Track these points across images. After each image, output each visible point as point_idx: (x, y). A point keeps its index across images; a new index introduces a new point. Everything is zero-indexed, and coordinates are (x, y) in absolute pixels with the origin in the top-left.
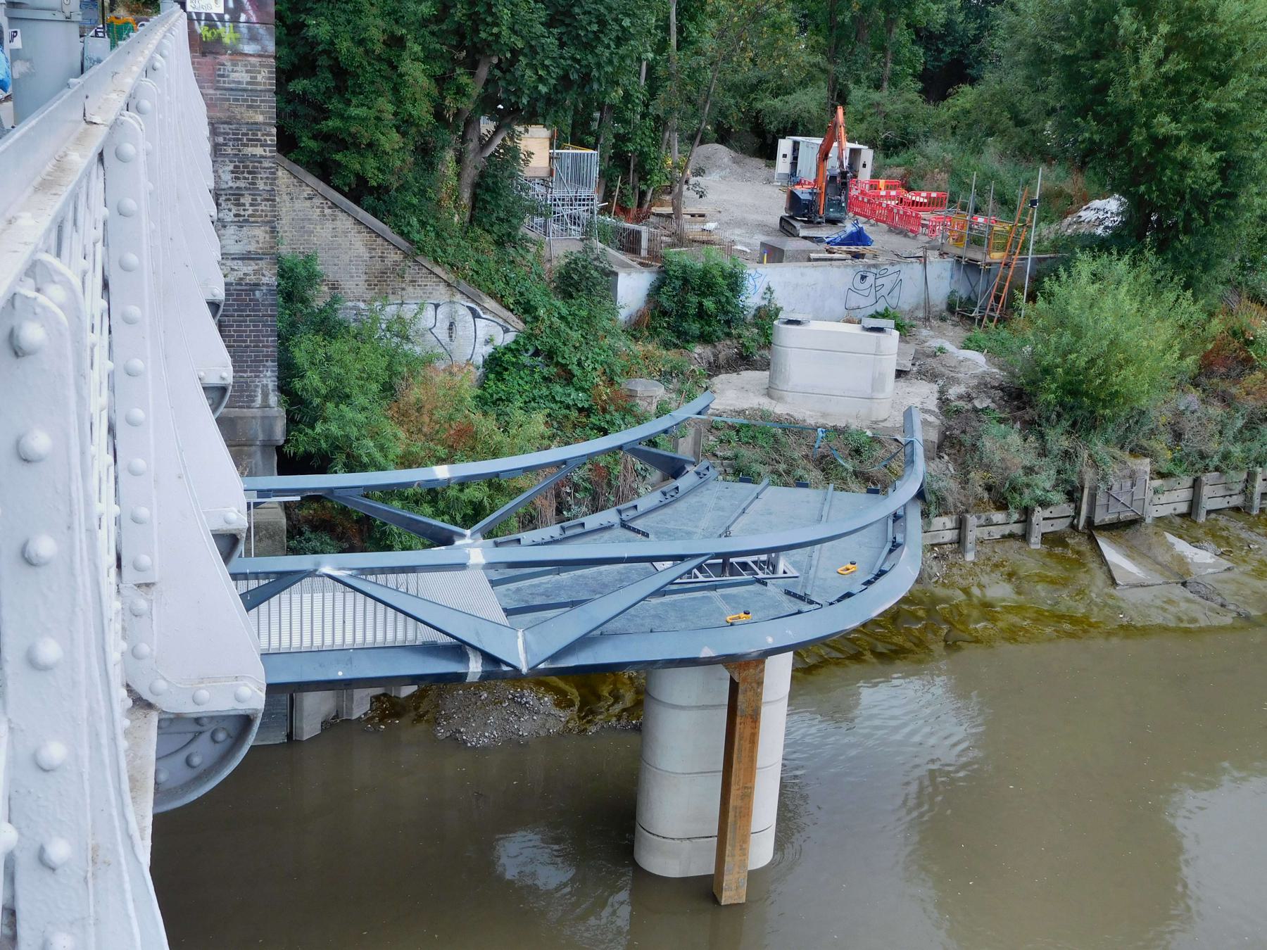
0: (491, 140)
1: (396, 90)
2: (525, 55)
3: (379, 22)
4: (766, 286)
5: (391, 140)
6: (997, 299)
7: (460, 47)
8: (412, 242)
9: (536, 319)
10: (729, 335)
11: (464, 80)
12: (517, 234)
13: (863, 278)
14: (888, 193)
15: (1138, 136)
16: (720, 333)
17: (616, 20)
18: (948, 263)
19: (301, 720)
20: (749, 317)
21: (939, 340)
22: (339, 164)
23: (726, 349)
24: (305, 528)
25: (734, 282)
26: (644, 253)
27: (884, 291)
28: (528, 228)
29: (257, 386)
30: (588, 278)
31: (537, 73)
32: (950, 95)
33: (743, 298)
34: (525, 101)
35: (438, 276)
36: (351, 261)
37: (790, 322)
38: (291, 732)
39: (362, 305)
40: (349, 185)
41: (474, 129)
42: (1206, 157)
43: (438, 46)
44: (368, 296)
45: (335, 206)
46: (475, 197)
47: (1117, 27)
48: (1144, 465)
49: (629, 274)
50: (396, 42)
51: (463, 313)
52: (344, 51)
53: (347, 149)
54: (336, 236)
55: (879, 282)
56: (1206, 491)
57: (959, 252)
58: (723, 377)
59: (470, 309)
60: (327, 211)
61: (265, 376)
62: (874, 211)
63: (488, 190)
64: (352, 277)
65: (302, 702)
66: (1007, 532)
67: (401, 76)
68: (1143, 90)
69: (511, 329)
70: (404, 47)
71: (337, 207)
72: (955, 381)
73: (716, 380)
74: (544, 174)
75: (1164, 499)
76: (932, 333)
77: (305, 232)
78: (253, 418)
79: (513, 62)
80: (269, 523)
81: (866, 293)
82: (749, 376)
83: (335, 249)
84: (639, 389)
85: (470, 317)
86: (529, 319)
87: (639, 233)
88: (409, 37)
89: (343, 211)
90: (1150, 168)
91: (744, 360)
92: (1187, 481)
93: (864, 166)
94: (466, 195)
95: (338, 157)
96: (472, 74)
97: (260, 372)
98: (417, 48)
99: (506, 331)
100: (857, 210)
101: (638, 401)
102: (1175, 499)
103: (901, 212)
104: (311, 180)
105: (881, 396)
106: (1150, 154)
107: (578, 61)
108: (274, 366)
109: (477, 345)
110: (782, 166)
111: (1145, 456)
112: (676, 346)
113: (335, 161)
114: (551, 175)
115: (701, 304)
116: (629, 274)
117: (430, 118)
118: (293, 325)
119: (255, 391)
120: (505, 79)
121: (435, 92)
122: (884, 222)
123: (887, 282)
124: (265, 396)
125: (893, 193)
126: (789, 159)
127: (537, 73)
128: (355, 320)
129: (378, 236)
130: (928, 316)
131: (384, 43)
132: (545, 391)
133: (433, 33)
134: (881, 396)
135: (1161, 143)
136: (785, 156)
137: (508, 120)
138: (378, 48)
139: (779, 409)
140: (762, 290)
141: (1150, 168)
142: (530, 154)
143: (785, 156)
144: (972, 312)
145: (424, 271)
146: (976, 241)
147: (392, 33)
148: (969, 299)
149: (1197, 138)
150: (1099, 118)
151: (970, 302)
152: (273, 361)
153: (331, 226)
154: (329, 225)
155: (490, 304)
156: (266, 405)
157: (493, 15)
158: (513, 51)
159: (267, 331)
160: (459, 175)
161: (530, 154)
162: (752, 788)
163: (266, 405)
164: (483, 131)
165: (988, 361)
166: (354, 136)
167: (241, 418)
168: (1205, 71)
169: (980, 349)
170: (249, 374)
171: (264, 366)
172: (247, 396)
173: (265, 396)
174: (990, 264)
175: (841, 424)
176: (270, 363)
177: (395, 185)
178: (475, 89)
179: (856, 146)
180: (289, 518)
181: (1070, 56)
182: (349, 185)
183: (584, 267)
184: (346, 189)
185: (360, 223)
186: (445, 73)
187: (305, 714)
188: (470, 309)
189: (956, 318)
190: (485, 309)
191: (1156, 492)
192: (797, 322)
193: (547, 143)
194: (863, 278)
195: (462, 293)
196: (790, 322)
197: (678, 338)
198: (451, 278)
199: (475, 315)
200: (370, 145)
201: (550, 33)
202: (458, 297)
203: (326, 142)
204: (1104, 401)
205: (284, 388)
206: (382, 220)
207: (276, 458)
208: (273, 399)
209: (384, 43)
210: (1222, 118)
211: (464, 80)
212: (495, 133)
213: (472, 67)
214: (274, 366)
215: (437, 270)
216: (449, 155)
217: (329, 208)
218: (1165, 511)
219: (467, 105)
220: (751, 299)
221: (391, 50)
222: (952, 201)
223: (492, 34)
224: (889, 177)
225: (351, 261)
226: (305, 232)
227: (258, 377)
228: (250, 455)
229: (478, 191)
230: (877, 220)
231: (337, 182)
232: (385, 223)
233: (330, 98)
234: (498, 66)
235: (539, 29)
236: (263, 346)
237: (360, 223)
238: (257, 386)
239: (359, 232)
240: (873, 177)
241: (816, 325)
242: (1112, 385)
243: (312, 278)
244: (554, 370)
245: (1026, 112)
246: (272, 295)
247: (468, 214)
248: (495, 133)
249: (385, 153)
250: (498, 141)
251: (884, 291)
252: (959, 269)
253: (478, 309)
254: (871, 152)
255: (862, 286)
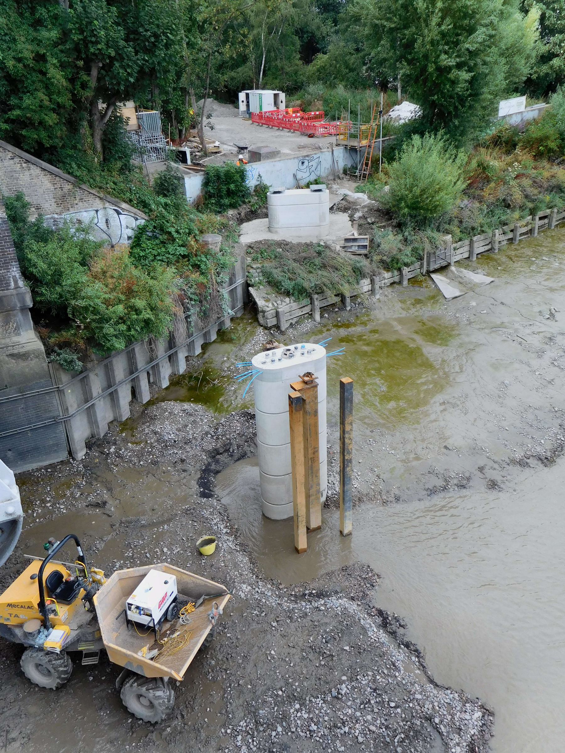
0: (106, 112)
1: (47, 87)
2: (117, 60)
3: (29, 47)
4: (258, 174)
5: (51, 119)
6: (367, 165)
7: (79, 58)
8: (76, 177)
9: (151, 210)
10: (244, 202)
11: (85, 78)
12: (129, 165)
13: (303, 163)
14: (296, 115)
15: (431, 68)
16: (240, 203)
17: (164, 33)
18: (341, 149)
19: (74, 444)
20: (252, 191)
21: (343, 190)
22: (24, 137)
23: (244, 210)
24: (56, 348)
25: (242, 174)
26: (189, 162)
27: (313, 169)
28: (135, 161)
29: (10, 277)
30: (172, 184)
31: (126, 71)
32: (314, 59)
33: (247, 182)
34: (122, 88)
35: (94, 195)
36: (44, 192)
37: (275, 193)
38: (70, 451)
39: (56, 216)
40: (34, 148)
41: (95, 107)
42: (465, 75)
43: (66, 59)
44: (58, 210)
45: (27, 161)
46: (104, 147)
47: (416, 9)
48: (449, 237)
49: (190, 178)
50: (40, 58)
51: (111, 213)
52: (11, 68)
53: (27, 127)
54: (32, 179)
55: (310, 164)
56: (476, 245)
57: (345, 143)
58: (245, 225)
59: (115, 210)
60: (24, 165)
61: (13, 271)
62: (291, 125)
63: (110, 142)
64: (47, 201)
65: (73, 436)
66: (392, 281)
67: (49, 79)
68: (432, 42)
69: (139, 218)
70: (45, 61)
71: (29, 162)
72: (357, 210)
73: (242, 226)
74: (136, 127)
75: (458, 252)
76: (338, 186)
77: (14, 179)
78: (11, 295)
79: (111, 65)
80: (34, 350)
81: (305, 171)
82: (256, 223)
83: (33, 186)
84: (210, 240)
85: (116, 215)
86: (147, 211)
87: (185, 152)
88: (48, 54)
89: (33, 164)
90: (436, 85)
91: (253, 215)
92: (467, 242)
93: (282, 102)
94: (99, 146)
95: (24, 132)
96: (89, 75)
97: (9, 269)
98: (55, 61)
99: (136, 219)
100: (283, 125)
101: (210, 247)
102: (462, 253)
103: (306, 124)
104: (10, 147)
105: (324, 224)
106: (437, 78)
107: (147, 61)
108: (17, 265)
109: (123, 230)
110: (242, 107)
111: (448, 233)
112: (220, 212)
113: (21, 135)
114: (140, 128)
115: (229, 189)
116: (190, 178)
117: (71, 102)
118: (21, 235)
119: (9, 280)
120: (108, 75)
121: (70, 86)
122: (298, 130)
123: (314, 163)
124: (16, 282)
125: (299, 115)
126: (245, 103)
127: (126, 71)
128: (54, 225)
129: (56, 176)
130: (336, 177)
131: (34, 59)
132: (163, 250)
133: (62, 51)
134: (324, 224)
135: (443, 71)
136: (243, 101)
137: (113, 100)
138: (31, 63)
139: (276, 237)
140: (256, 176)
141: (436, 85)
142: (128, 118)
143: (243, 101)
144: (355, 173)
145: (86, 192)
146: (353, 136)
147: (38, 52)
148: (352, 166)
149: (459, 66)
150: (410, 62)
151: (354, 168)
152: (15, 262)
153: (28, 174)
154: (27, 173)
155: (124, 205)
156: (17, 287)
157: (95, 36)
158: (110, 57)
159: (8, 245)
160: (92, 135)
161: (128, 118)
162: (318, 448)
163: (17, 287)
164: (100, 108)
165: (369, 197)
166: (29, 119)
167: (5, 296)
168: (462, 28)
169: (363, 192)
170: (3, 271)
171: (11, 265)
172: (5, 283)
173: (16, 282)
174: (361, 147)
175: (308, 242)
176: (14, 263)
177: (61, 144)
178: (93, 84)
179: (276, 92)
180: (44, 344)
181: (393, 28)
182: (34, 148)
183: (169, 178)
184: (32, 150)
185: (45, 170)
186: (73, 76)
187: (76, 441)
188: (115, 210)
189: (348, 177)
190: (122, 209)
191: (455, 249)
192: (279, 192)
193: (134, 110)
194: (303, 163)
195: (109, 202)
196: (275, 193)
197: (220, 208)
198: (102, 195)
199: (119, 213)
200: (41, 123)
201: (128, 45)
202: (107, 205)
203: (14, 124)
204: (431, 210)
205: (27, 275)
206: (56, 166)
207: (30, 314)
208: (21, 283)
209: (34, 59)
210: (473, 54)
211: (85, 78)
212: (107, 109)
213: (88, 70)
214: (17, 265)
215: (93, 191)
216: (85, 123)
217: (25, 163)
218: (458, 258)
219: (89, 93)
220: (251, 183)
221: (39, 63)
222: (326, 115)
223: (98, 49)
224: (293, 107)
225: (44, 192)
226: (14, 179)
227: (9, 272)
228: (15, 316)
229: (106, 143)
230: (294, 130)
231: (26, 147)
232: (58, 168)
233: (9, 97)
234: (103, 68)
235: (122, 43)
236: (8, 254)
237: (45, 170)
238: (10, 277)
239: (45, 175)
240: (286, 107)
241: (287, 192)
242: (435, 202)
243: (25, 206)
244: (166, 237)
245: (353, 64)
246: (5, 224)
247: (102, 157)
248: (107, 109)
249: (50, 126)
250: (110, 113)
251: (313, 169)
252: (347, 152)
253: (119, 210)
254: (284, 94)
255: (302, 168)
